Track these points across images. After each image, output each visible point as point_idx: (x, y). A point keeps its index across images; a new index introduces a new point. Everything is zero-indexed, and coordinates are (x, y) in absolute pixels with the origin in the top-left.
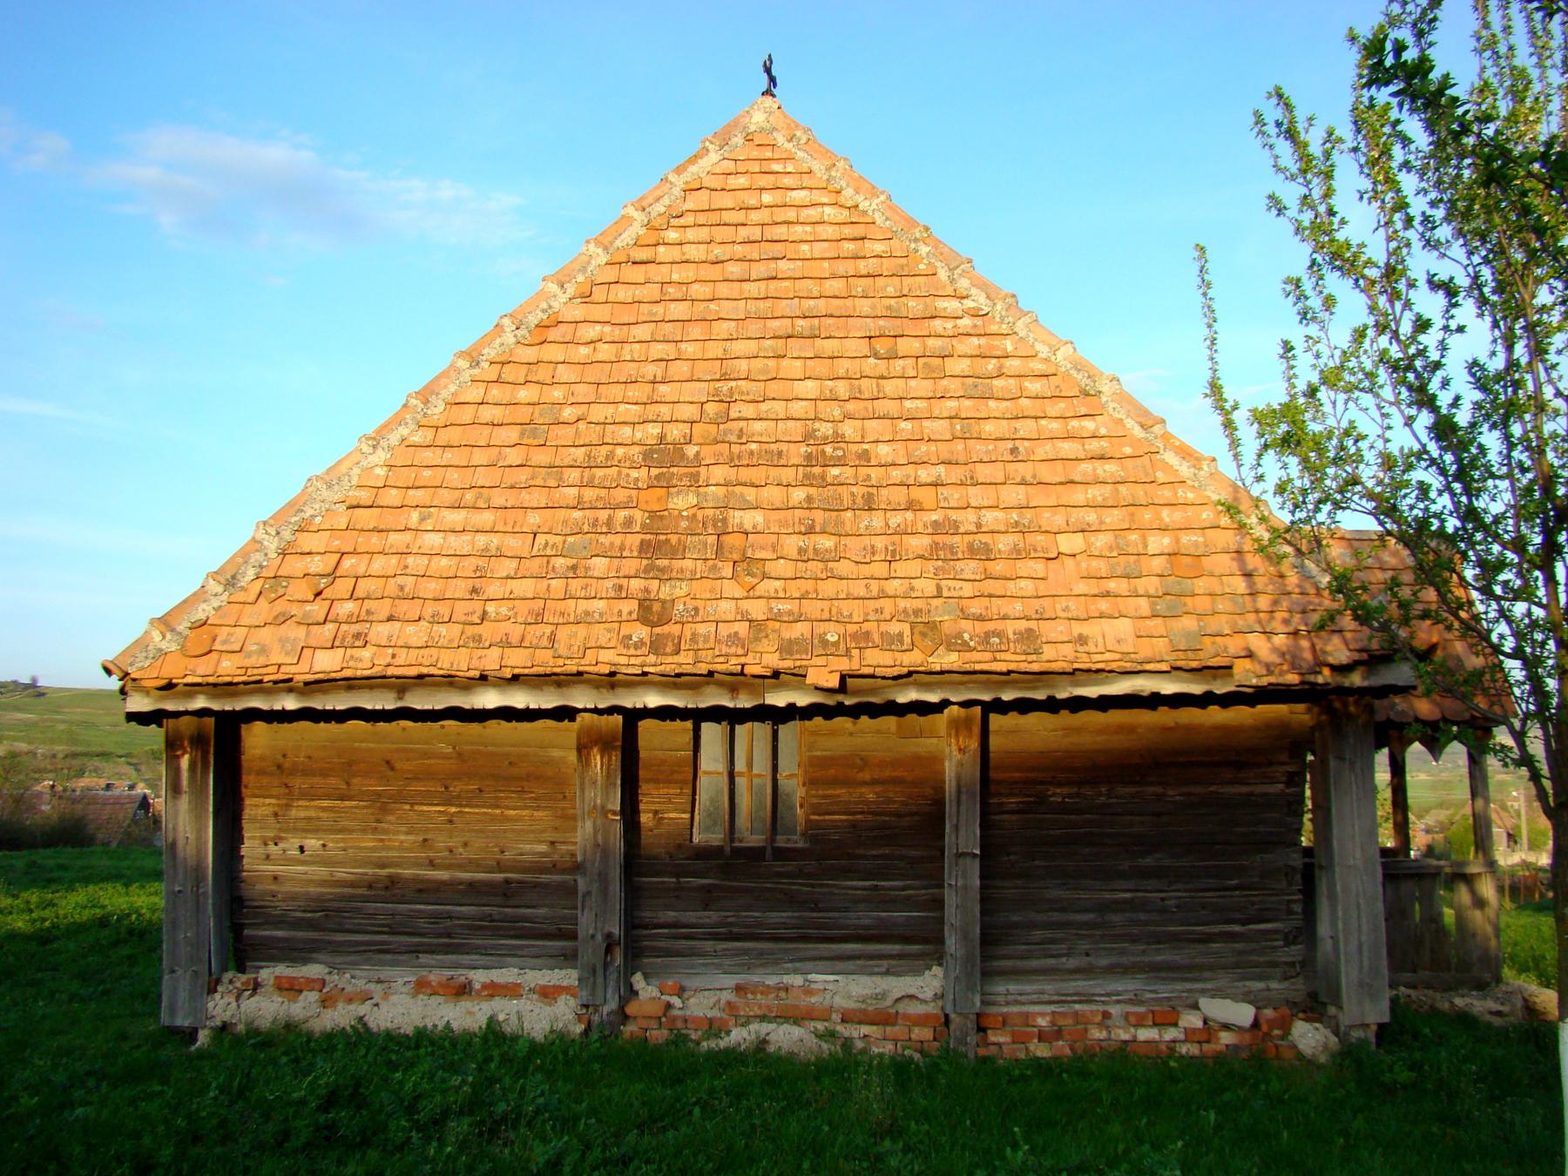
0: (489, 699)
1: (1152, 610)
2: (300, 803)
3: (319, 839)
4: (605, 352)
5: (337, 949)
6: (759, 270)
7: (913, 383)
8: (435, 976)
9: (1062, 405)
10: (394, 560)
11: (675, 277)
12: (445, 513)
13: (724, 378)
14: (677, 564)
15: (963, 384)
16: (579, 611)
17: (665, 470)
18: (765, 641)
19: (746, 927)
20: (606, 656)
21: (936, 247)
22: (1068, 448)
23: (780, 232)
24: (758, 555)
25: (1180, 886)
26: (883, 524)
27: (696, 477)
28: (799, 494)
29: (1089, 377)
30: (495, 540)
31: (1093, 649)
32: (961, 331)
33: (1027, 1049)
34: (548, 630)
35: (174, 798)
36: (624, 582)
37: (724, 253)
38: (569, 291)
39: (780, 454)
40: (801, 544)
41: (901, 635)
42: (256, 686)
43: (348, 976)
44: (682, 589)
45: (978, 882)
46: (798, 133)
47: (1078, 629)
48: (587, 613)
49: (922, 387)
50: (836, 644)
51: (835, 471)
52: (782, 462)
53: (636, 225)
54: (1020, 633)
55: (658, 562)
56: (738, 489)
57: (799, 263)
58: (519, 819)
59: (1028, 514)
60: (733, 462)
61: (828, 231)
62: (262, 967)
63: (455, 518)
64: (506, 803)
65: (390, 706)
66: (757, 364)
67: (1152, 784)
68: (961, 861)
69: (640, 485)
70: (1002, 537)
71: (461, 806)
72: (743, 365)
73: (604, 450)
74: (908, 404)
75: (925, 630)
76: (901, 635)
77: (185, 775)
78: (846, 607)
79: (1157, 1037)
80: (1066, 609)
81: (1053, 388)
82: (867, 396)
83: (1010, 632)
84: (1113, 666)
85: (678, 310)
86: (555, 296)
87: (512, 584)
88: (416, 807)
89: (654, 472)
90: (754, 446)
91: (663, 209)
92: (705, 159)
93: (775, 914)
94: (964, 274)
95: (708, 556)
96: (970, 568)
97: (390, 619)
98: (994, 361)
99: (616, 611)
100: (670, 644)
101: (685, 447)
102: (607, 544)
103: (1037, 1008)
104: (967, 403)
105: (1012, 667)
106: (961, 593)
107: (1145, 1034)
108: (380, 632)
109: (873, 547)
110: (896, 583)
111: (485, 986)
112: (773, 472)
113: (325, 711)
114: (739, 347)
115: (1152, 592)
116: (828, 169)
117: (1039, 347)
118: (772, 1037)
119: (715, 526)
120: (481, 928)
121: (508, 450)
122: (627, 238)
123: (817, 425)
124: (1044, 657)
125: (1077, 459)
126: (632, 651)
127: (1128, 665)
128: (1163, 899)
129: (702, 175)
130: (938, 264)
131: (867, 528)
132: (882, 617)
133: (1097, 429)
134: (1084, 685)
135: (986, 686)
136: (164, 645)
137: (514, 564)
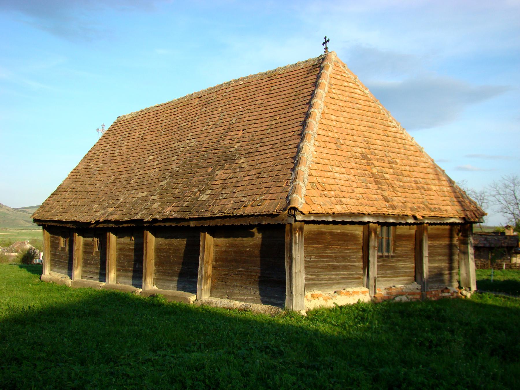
2: (310, 246)
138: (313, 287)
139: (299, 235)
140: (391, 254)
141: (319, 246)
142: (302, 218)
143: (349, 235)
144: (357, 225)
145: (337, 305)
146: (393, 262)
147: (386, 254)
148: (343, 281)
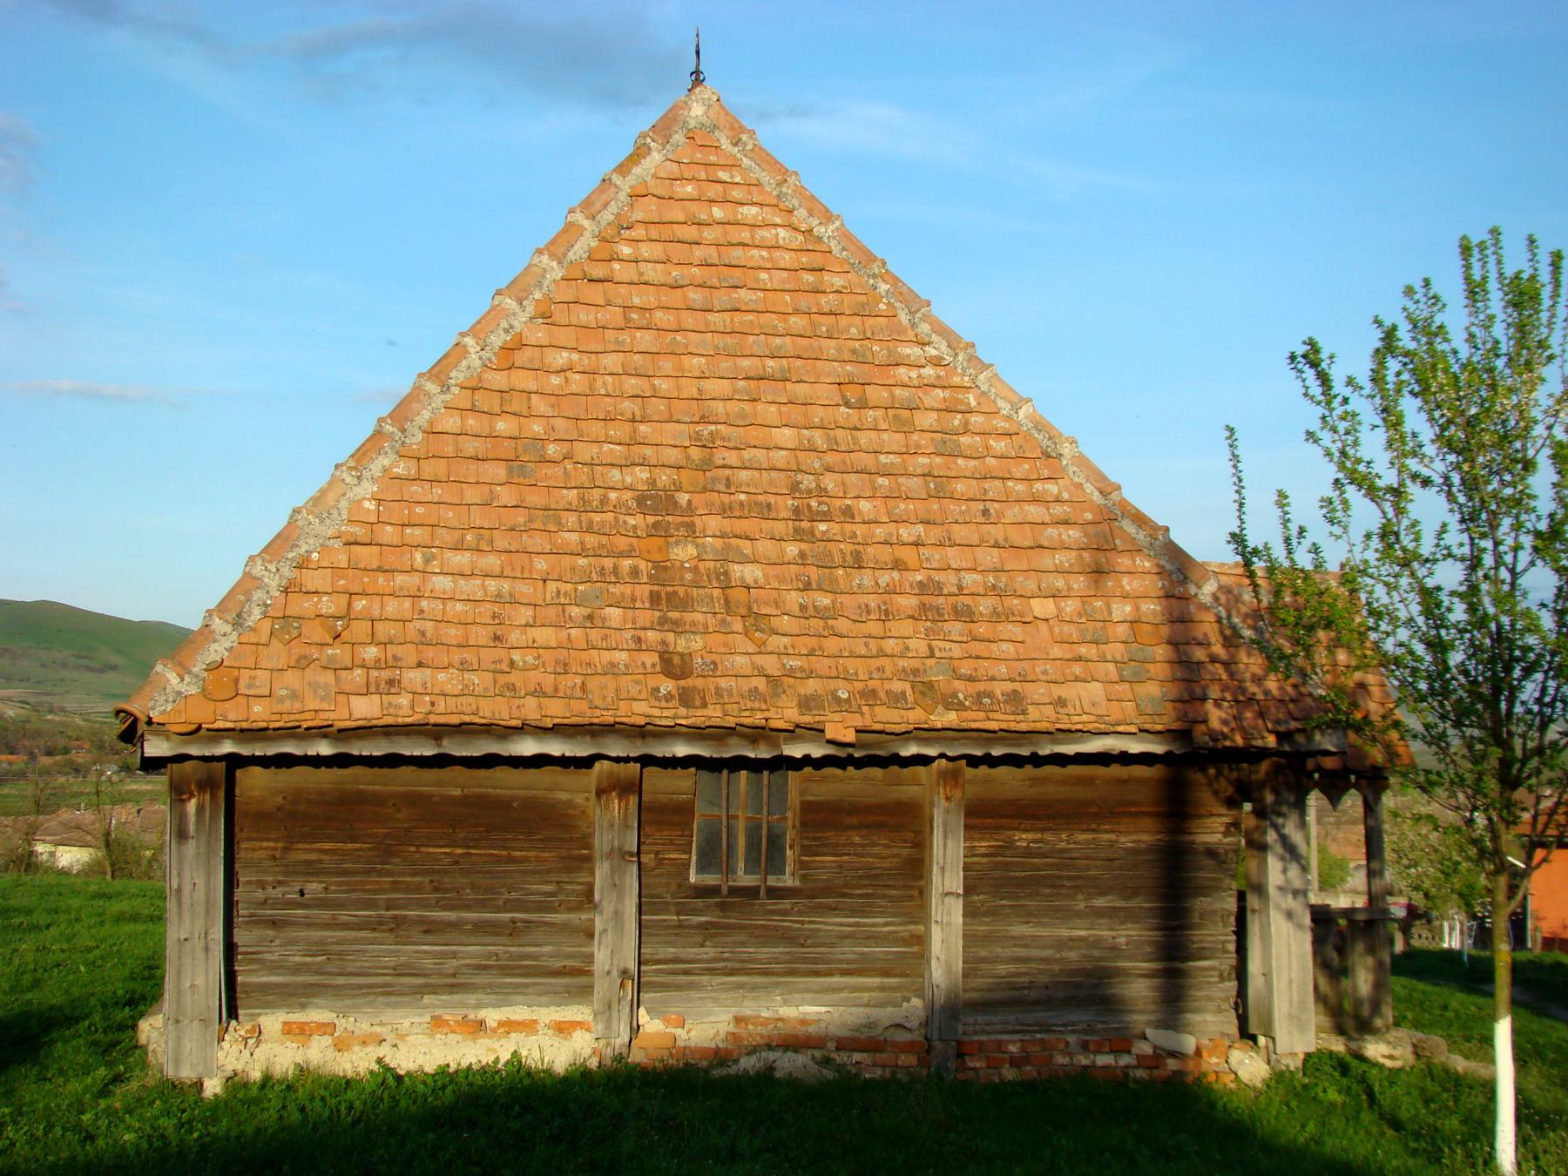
0: (528, 747)
1: (1121, 676)
2: (300, 846)
3: (320, 882)
4: (577, 382)
5: (338, 992)
6: (721, 298)
7: (885, 436)
8: (450, 1016)
9: (1026, 466)
10: (407, 603)
11: (636, 301)
12: (448, 554)
13: (704, 420)
14: (689, 617)
15: (932, 439)
16: (604, 662)
17: (660, 518)
18: (784, 696)
19: (743, 961)
20: (640, 707)
21: (894, 286)
22: (1035, 513)
23: (737, 254)
24: (764, 611)
25: (1130, 925)
26: (873, 583)
27: (691, 527)
28: (792, 550)
29: (1050, 438)
30: (506, 586)
31: (1072, 711)
32: (926, 382)
33: (1000, 1073)
34: (578, 681)
35: (180, 843)
36: (641, 633)
37: (683, 276)
38: (528, 309)
39: (769, 505)
40: (801, 600)
41: (903, 693)
42: (291, 732)
43: (352, 1019)
44: (697, 643)
45: (961, 920)
46: (744, 137)
47: (1058, 691)
48: (613, 665)
49: (893, 440)
50: (848, 701)
51: (823, 527)
52: (773, 515)
53: (587, 234)
54: (1008, 694)
55: (670, 614)
56: (734, 541)
57: (760, 294)
58: (525, 860)
59: (1004, 578)
60: (724, 511)
61: (786, 259)
62: (260, 1015)
63: (460, 560)
64: (513, 844)
65: (429, 752)
66: (733, 407)
67: (1106, 832)
68: (947, 900)
69: (639, 533)
70: (981, 600)
71: (468, 847)
72: (720, 407)
73: (597, 493)
74: (882, 458)
75: (924, 689)
76: (903, 693)
77: (192, 818)
78: (852, 665)
79: (1113, 1062)
80: (1045, 672)
81: (1016, 448)
82: (843, 449)
83: (998, 693)
84: (1090, 727)
85: (644, 339)
86: (514, 314)
87: (534, 633)
88: (422, 849)
89: (651, 519)
90: (742, 497)
91: (612, 218)
92: (648, 159)
93: (767, 950)
94: (925, 318)
95: (717, 610)
96: (956, 628)
97: (420, 665)
98: (959, 416)
99: (639, 663)
100: (697, 697)
101: (677, 494)
102: (618, 594)
103: (1005, 1037)
104: (938, 460)
105: (1004, 726)
106: (951, 654)
107: (1103, 1060)
108: (413, 677)
109: (867, 606)
110: (892, 642)
111: (501, 1024)
112: (765, 525)
113: (361, 757)
114: (712, 386)
115: (1119, 658)
116: (779, 184)
117: (1001, 403)
118: (778, 1064)
119: (718, 579)
120: (486, 967)
121: (499, 488)
122: (578, 251)
123: (800, 477)
124: (1030, 717)
125: (1043, 524)
126: (664, 704)
127: (1102, 726)
128: (1114, 938)
129: (648, 179)
130: (898, 305)
131: (859, 586)
132: (885, 676)
133: (1060, 492)
134: (1061, 743)
135: (977, 742)
136: (183, 688)
137: (530, 612)
138: (314, 995)
139: (200, 809)
140: (788, 880)
141: (350, 846)
142: (171, 749)
143: (515, 805)
144: (559, 768)
145: (387, 1068)
146: (785, 913)
147: (744, 879)
148: (480, 980)
